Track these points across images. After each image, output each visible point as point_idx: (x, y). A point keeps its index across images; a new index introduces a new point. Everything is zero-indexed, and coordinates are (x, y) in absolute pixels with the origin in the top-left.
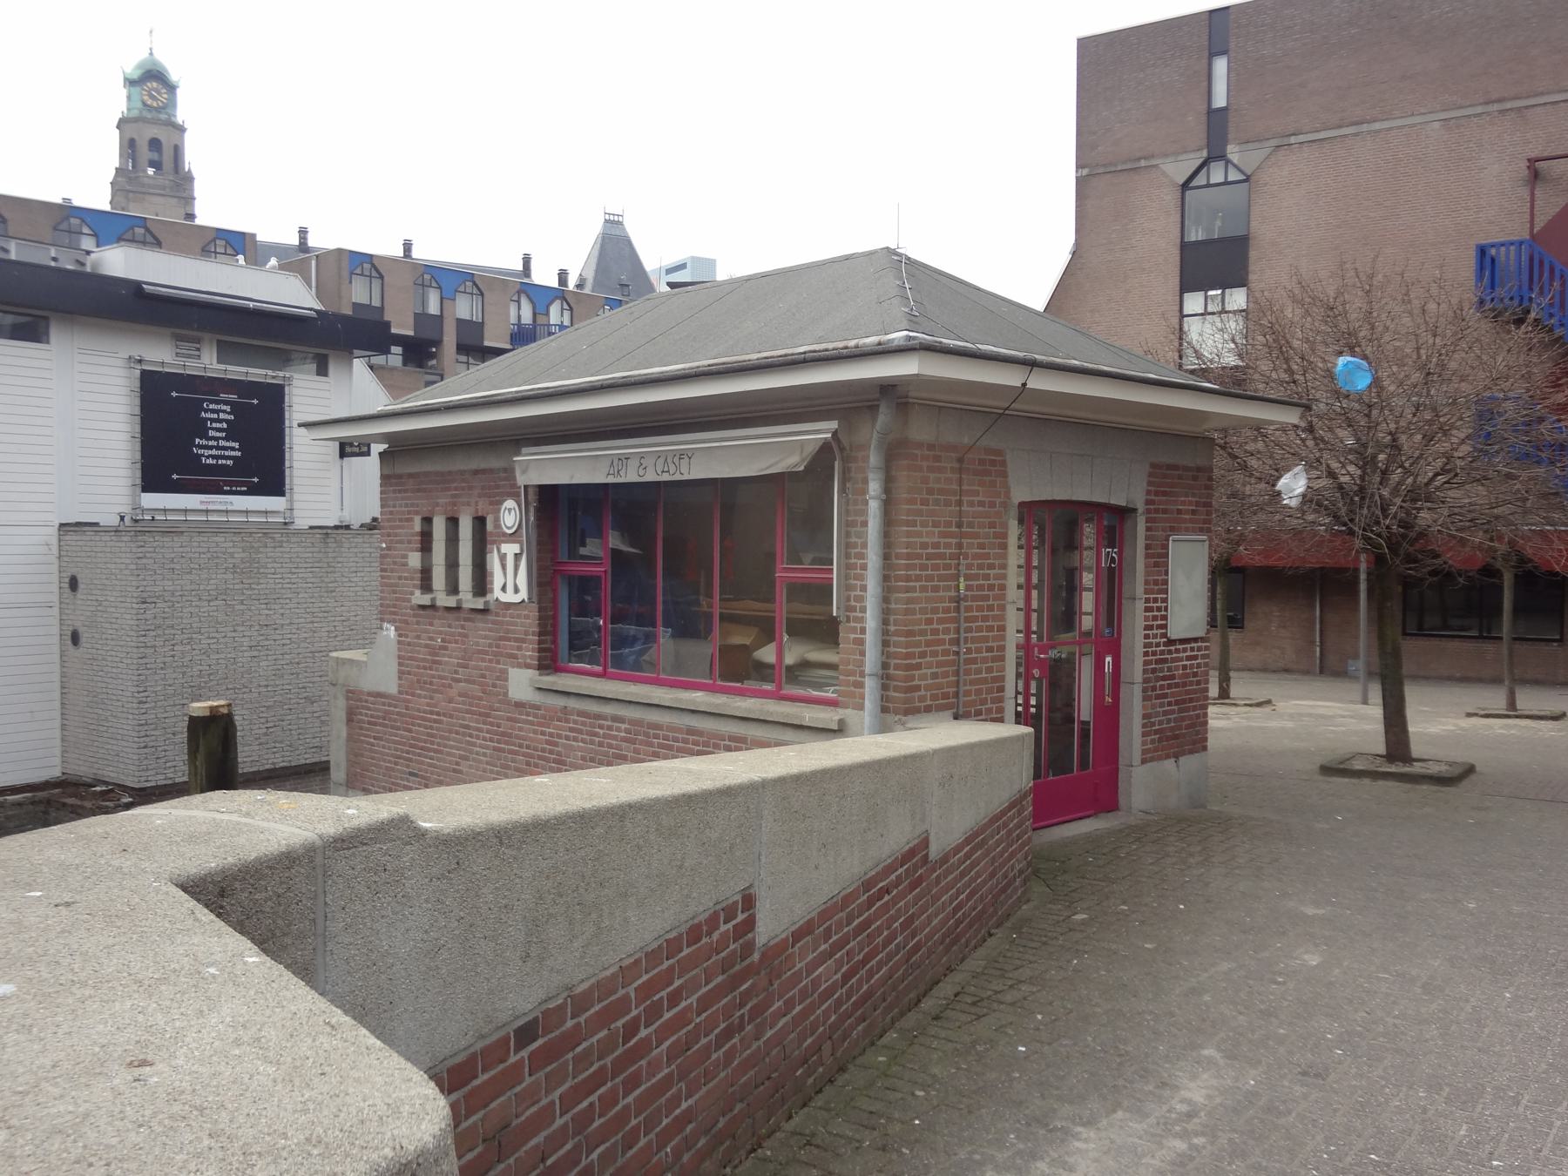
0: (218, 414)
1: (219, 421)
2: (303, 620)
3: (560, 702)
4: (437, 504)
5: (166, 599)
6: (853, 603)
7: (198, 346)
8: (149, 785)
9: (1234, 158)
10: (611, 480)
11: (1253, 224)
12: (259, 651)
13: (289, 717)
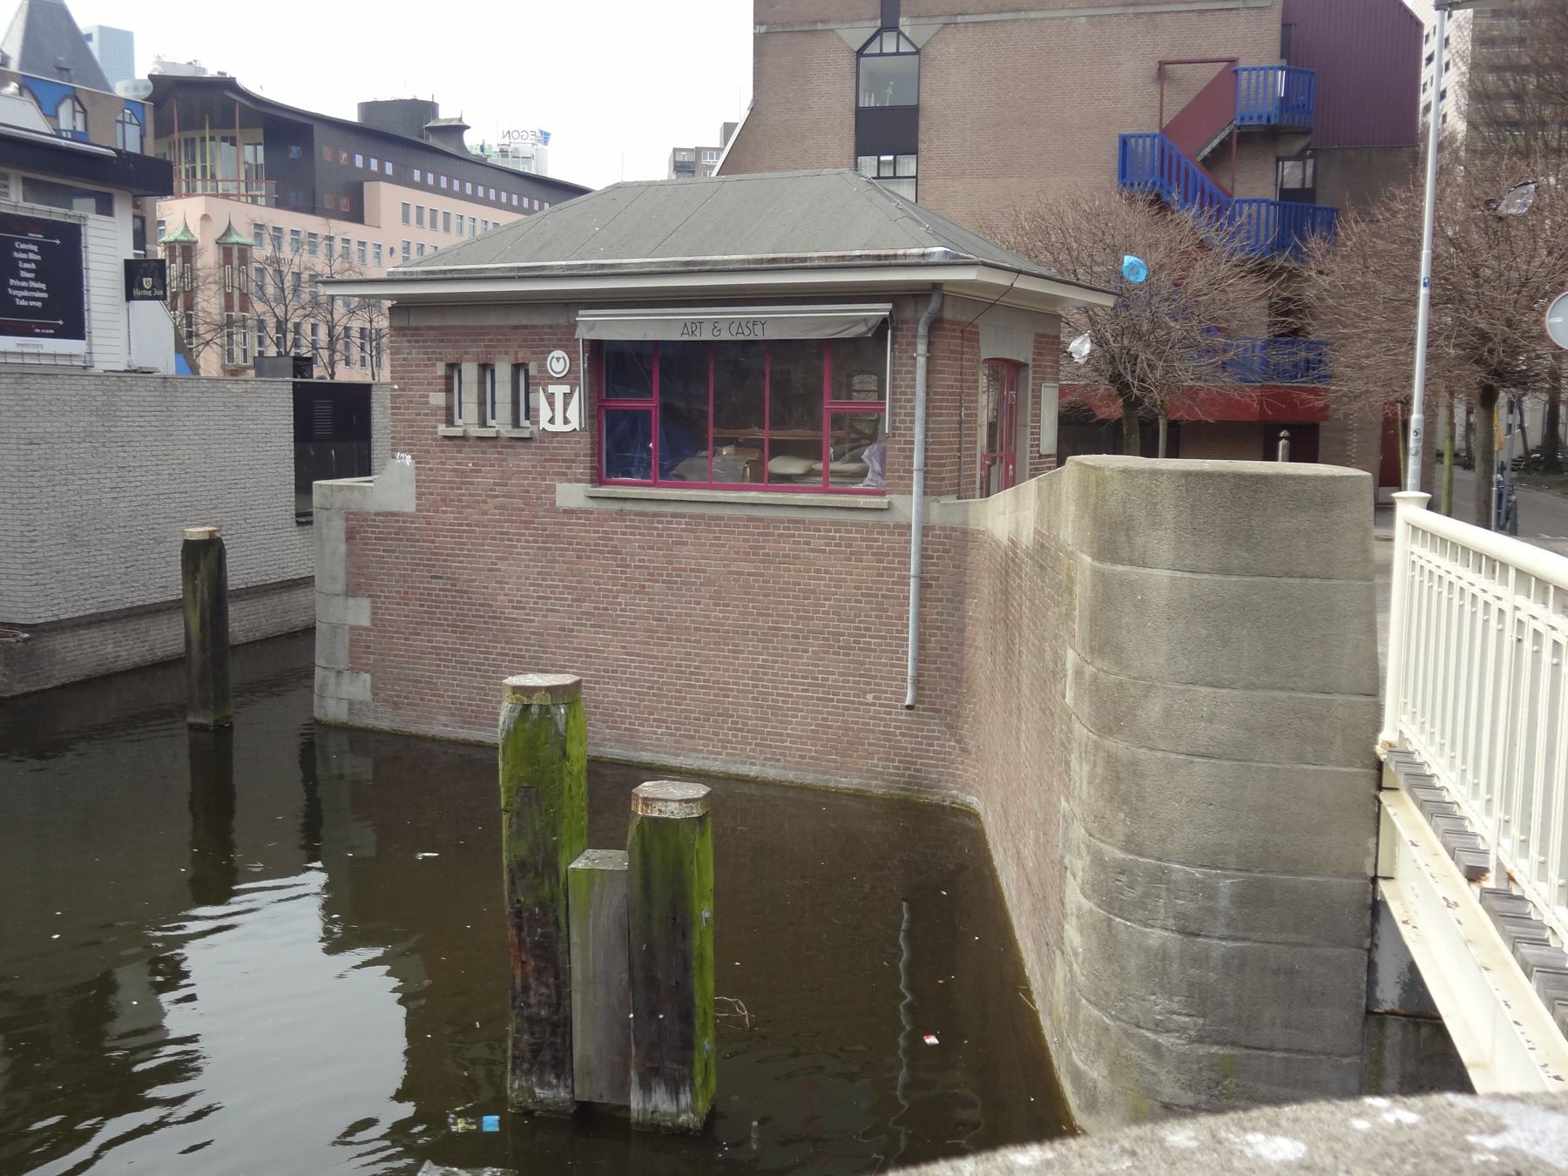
0: (27, 253)
1: (28, 261)
2: (149, 463)
3: (617, 506)
4: (467, 353)
5: (48, 440)
6: (898, 425)
7: (5, 183)
8: (40, 621)
9: (906, 30)
10: (686, 338)
11: (924, 96)
12: (118, 492)
13: (142, 557)
